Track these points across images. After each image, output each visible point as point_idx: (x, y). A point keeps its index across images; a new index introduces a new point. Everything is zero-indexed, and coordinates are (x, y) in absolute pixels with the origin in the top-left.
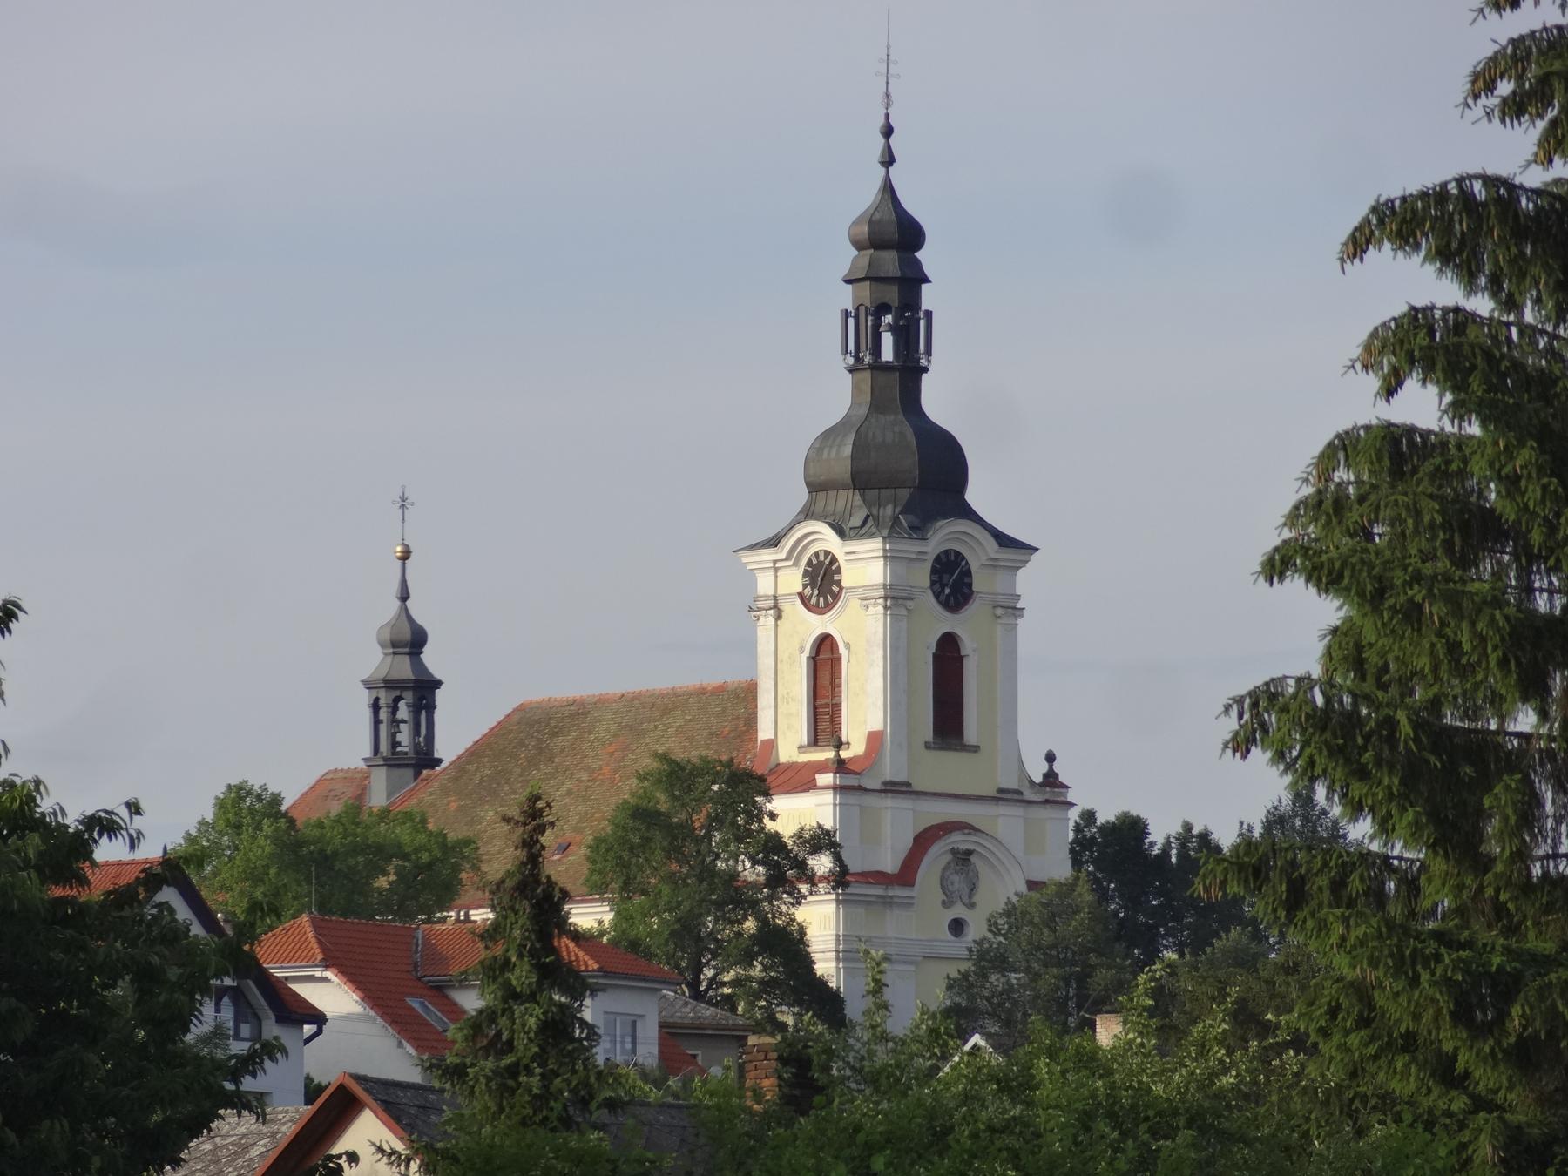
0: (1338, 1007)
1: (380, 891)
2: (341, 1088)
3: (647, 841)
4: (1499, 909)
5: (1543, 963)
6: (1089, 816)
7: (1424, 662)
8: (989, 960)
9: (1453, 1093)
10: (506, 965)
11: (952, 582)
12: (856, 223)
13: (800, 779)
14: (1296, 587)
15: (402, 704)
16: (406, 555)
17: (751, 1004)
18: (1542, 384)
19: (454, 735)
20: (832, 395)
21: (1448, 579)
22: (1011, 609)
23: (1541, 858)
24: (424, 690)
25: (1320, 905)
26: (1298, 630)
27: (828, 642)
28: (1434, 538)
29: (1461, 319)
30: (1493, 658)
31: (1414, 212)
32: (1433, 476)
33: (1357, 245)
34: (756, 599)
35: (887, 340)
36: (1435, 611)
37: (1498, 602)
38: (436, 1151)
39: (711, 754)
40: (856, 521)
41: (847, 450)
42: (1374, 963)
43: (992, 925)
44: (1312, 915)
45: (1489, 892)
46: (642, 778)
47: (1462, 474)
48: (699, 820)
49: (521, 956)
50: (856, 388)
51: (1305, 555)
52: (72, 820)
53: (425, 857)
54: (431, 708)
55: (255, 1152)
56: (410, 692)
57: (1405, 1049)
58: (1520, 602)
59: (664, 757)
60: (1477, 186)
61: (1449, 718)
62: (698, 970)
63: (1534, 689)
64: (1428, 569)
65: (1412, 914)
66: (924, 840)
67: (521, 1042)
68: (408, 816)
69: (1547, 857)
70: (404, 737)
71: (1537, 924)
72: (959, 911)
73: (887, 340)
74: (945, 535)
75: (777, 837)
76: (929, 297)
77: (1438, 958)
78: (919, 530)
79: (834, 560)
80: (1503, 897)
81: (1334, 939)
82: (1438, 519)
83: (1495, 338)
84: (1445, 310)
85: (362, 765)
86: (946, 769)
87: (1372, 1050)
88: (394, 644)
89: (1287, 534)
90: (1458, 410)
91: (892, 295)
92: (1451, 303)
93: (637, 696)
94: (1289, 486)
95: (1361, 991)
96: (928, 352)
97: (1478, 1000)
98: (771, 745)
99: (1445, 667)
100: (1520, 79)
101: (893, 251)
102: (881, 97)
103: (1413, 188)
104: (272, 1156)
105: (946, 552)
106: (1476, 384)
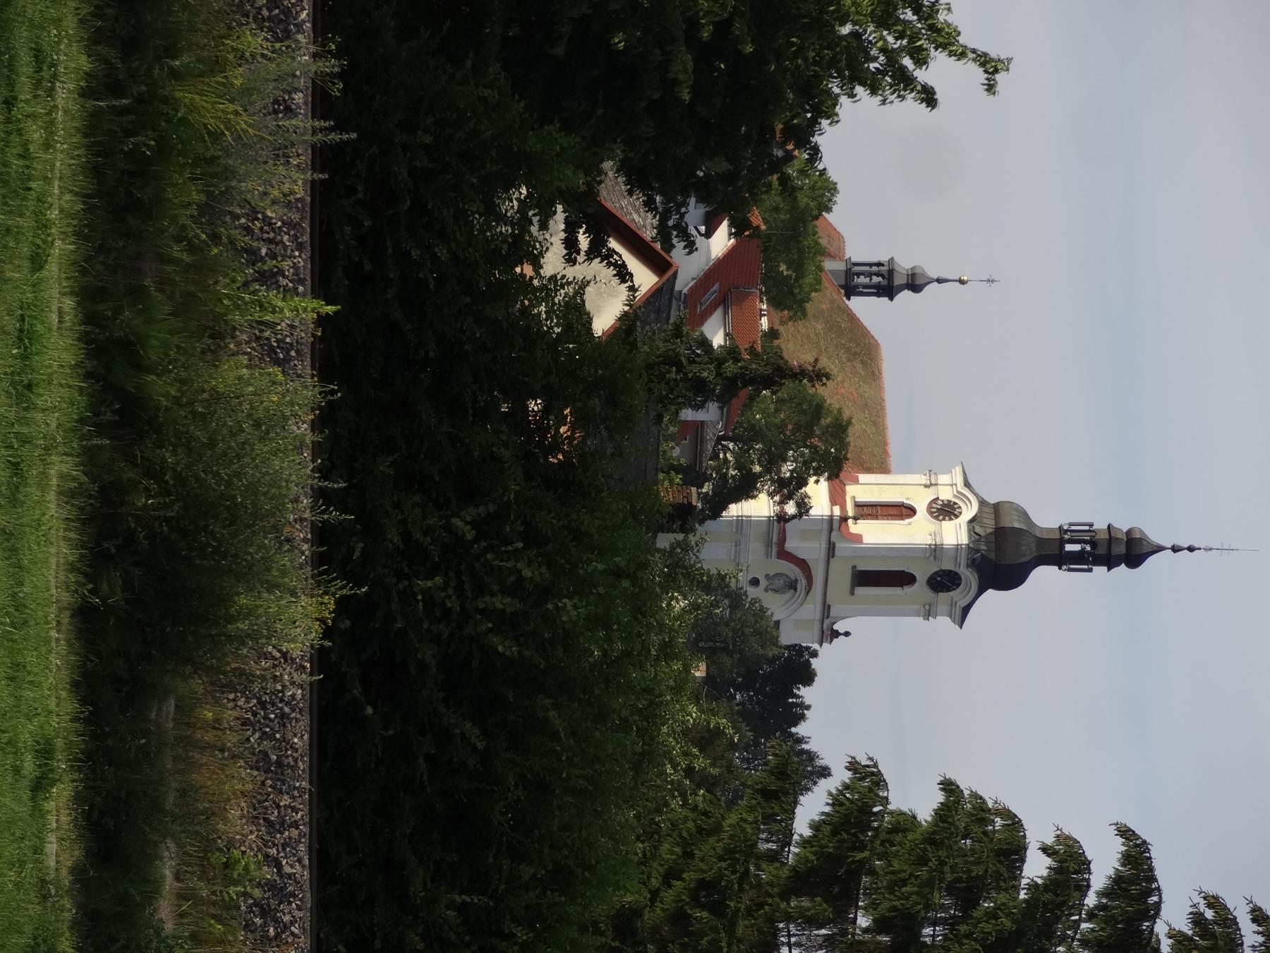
0: (709, 817)
1: (778, 266)
2: (670, 265)
3: (803, 412)
4: (761, 906)
5: (731, 930)
6: (814, 654)
7: (896, 865)
8: (736, 599)
9: (660, 879)
10: (737, 360)
11: (944, 581)
12: (1141, 531)
13: (837, 497)
14: (940, 797)
15: (880, 279)
16: (962, 282)
17: (713, 469)
18: (1047, 933)
19: (862, 306)
20: (1048, 516)
21: (941, 880)
22: (929, 613)
23: (788, 928)
24: (888, 291)
25: (763, 808)
26: (915, 797)
27: (909, 512)
28: (964, 872)
29: (1084, 888)
30: (897, 903)
31: (1141, 864)
32: (997, 872)
33: (1125, 833)
34: (936, 474)
35: (1076, 547)
36: (923, 873)
37: (928, 907)
38: (635, 321)
39: (851, 448)
40: (978, 530)
41: (1017, 525)
42: (731, 837)
43: (755, 601)
44: (759, 804)
45: (770, 901)
46: (839, 410)
47: (998, 889)
48: (815, 441)
49: (741, 368)
50: (1051, 530)
51: (954, 802)
52: (817, 139)
53: (796, 291)
54: (878, 295)
55: (635, 216)
56: (887, 282)
57: (685, 852)
58: (929, 919)
59: (849, 422)
60: (1155, 899)
61: (865, 880)
62: (731, 440)
63: (880, 925)
64: (947, 869)
65: (758, 858)
66: (803, 564)
67: (695, 368)
68: (819, 282)
69: (789, 931)
70: (863, 280)
71: (752, 926)
72: (763, 583)
73: (1076, 547)
74: (970, 578)
75: (806, 484)
76: (1100, 571)
77: (734, 872)
78: (972, 564)
79: (957, 517)
80: (767, 908)
81: (744, 815)
82: (973, 874)
83: (1073, 907)
84: (1088, 880)
85: (847, 257)
86: (841, 577)
87: (685, 834)
88: (913, 275)
89: (966, 793)
90: (1033, 887)
91: (1101, 551)
92: (1092, 883)
93: (883, 408)
94: (992, 794)
95: (716, 830)
96: (1070, 570)
97: (710, 893)
98: (856, 481)
99: (893, 878)
100: (1215, 922)
101: (1126, 550)
102: (1210, 546)
103: (1156, 864)
104: (633, 226)
105: (960, 578)
106: (1048, 897)
